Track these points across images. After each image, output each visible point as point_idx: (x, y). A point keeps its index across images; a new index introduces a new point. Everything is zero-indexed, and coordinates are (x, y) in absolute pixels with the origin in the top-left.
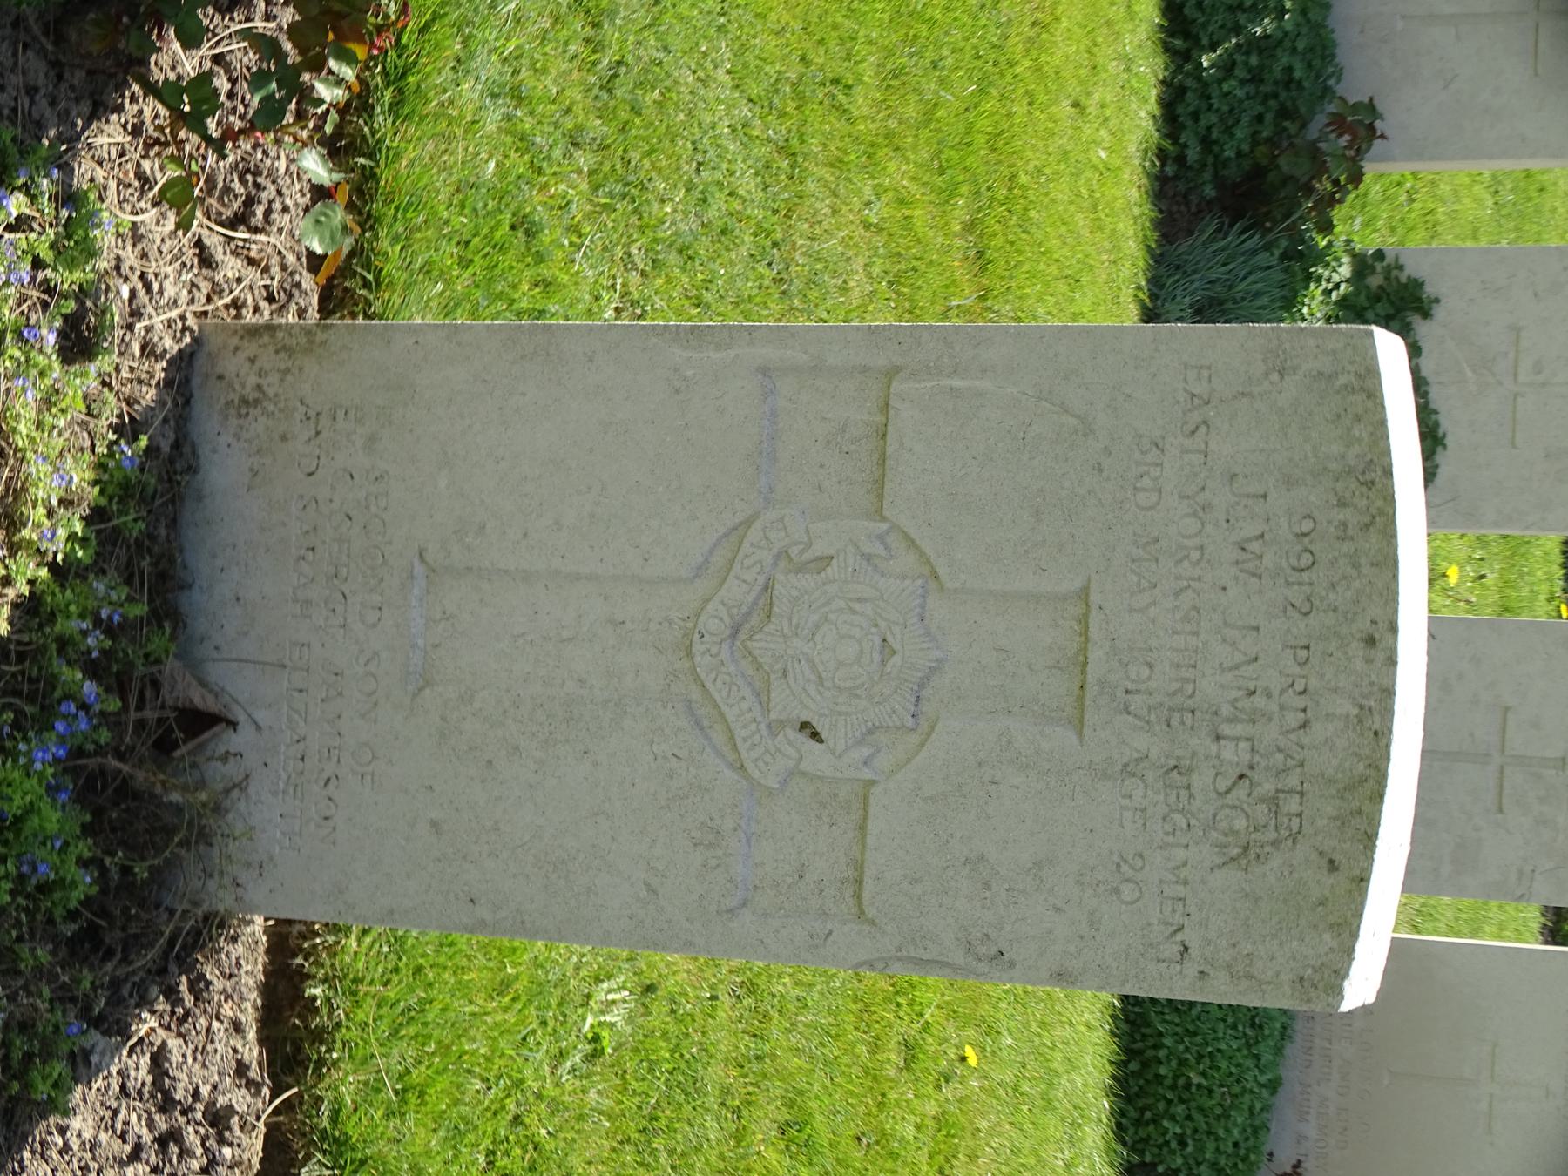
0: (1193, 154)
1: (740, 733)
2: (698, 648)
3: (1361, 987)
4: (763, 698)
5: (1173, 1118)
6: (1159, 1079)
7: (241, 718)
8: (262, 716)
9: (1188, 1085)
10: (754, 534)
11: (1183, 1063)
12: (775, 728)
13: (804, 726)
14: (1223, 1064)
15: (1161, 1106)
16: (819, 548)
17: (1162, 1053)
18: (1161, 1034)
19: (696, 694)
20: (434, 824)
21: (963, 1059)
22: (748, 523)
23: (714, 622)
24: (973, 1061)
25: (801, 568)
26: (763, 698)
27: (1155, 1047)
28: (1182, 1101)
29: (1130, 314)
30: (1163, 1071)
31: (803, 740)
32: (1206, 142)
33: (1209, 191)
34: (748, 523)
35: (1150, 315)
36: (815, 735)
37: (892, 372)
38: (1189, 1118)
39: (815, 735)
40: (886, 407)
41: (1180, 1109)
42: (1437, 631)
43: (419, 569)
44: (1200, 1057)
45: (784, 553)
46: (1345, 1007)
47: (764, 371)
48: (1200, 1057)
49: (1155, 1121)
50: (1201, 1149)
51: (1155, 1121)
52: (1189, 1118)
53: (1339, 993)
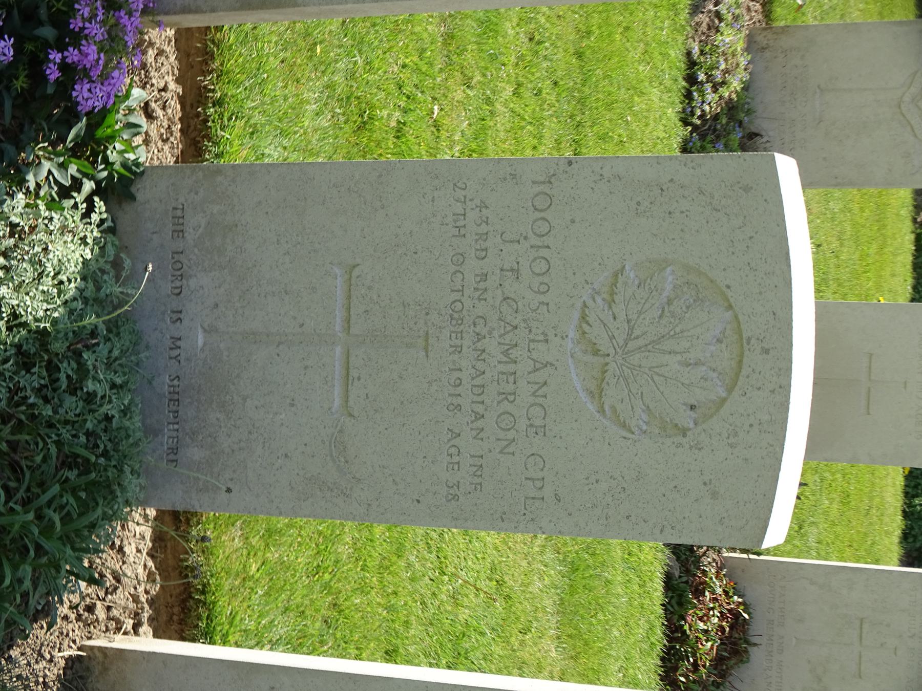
2: (902, 106)
7: (763, 133)
23: (907, 98)
43: (818, 91)
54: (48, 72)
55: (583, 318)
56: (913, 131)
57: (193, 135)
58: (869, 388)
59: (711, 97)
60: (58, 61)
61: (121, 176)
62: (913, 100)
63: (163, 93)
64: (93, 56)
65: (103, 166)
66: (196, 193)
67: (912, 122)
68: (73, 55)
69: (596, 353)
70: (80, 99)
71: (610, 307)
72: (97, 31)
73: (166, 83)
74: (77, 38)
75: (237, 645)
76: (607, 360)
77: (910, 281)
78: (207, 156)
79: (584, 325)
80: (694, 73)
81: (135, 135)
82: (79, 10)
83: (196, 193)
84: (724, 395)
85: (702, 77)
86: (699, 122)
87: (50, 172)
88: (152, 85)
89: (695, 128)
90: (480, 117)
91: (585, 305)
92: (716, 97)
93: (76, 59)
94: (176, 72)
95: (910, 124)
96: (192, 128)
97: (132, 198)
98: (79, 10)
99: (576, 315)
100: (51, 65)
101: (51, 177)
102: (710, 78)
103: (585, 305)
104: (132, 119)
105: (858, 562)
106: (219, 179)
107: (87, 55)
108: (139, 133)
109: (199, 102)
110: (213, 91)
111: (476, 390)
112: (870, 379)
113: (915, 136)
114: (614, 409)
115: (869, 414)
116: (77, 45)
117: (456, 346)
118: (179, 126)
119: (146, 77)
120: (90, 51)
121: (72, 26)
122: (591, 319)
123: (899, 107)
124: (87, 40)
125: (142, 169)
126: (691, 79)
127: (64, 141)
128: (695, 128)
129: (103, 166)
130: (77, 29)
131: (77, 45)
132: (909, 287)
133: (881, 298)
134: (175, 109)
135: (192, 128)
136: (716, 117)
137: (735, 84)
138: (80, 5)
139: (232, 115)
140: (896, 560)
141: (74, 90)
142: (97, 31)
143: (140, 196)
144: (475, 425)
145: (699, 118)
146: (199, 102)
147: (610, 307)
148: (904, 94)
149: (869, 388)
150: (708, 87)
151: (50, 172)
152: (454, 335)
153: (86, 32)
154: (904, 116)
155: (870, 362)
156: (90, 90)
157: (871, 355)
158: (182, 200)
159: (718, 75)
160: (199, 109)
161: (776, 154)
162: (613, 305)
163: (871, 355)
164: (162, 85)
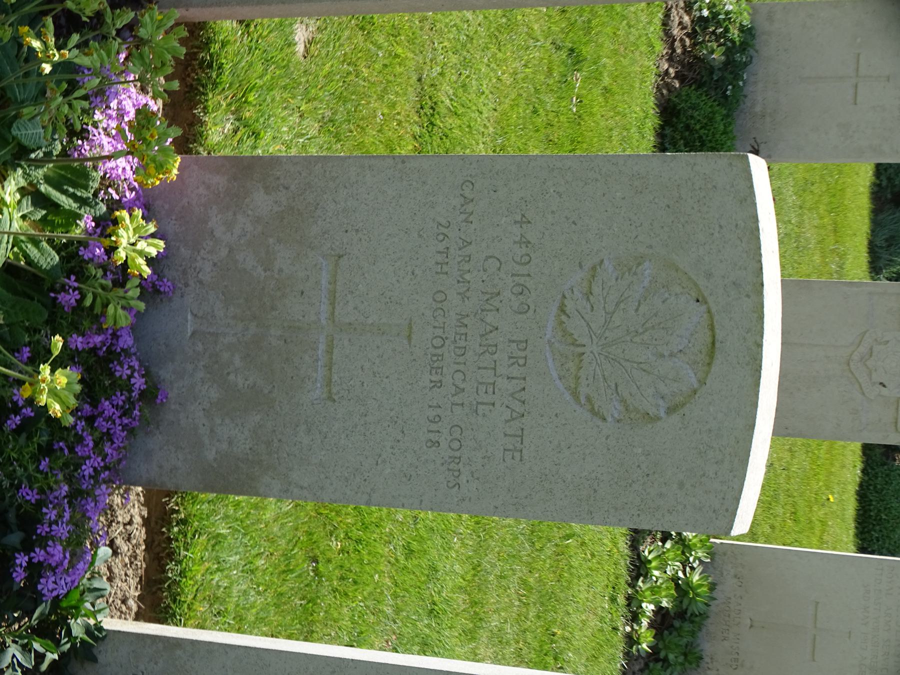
0: (884, 183)
2: (851, 364)
5: (875, 531)
6: (870, 516)
9: (881, 519)
10: (867, 335)
11: (879, 511)
13: (881, 383)
14: (893, 512)
15: (871, 526)
17: (872, 507)
18: (871, 501)
19: (850, 375)
21: (829, 499)
22: (865, 332)
23: (856, 357)
24: (832, 500)
25: (880, 344)
27: (870, 505)
28: (878, 525)
29: (643, 140)
30: (872, 514)
31: (881, 387)
32: (889, 179)
33: (889, 196)
34: (865, 332)
35: (662, 146)
36: (884, 386)
38: (881, 531)
39: (884, 386)
41: (878, 528)
44: (885, 509)
45: (876, 340)
48: (885, 509)
49: (868, 532)
50: (884, 543)
51: (868, 532)
52: (881, 531)
54: (14, 575)
55: (562, 310)
56: (861, 389)
57: (158, 550)
58: (815, 636)
60: (24, 564)
61: (83, 641)
62: (862, 359)
63: (128, 527)
64: (58, 556)
65: (66, 639)
66: (156, 663)
67: (860, 380)
68: (39, 555)
69: (574, 344)
70: (45, 591)
71: (588, 299)
72: (63, 530)
73: (132, 516)
74: (43, 542)
77: (859, 466)
78: (170, 575)
79: (563, 318)
81: (98, 597)
82: (46, 514)
83: (156, 663)
84: (696, 386)
87: (14, 656)
88: (118, 523)
89: (681, 63)
93: (42, 559)
94: (142, 499)
96: (156, 543)
97: (94, 660)
98: (46, 514)
99: (554, 310)
100: (18, 569)
101: (15, 660)
104: (96, 584)
106: (179, 652)
107: (53, 556)
108: (102, 596)
109: (163, 520)
110: (178, 512)
111: (459, 352)
112: (815, 627)
113: (863, 394)
114: (588, 399)
115: (814, 660)
116: (44, 547)
118: (144, 547)
119: (112, 516)
120: (56, 552)
121: (39, 531)
123: (848, 365)
124: (53, 541)
125: (104, 634)
127: (30, 615)
129: (66, 639)
130: (44, 534)
131: (44, 547)
133: (830, 497)
134: (140, 534)
135: (156, 543)
138: (48, 508)
139: (196, 531)
141: (40, 583)
142: (63, 530)
143: (101, 658)
146: (163, 520)
147: (588, 299)
149: (815, 636)
151: (14, 656)
153: (53, 533)
154: (852, 373)
155: (816, 610)
156: (55, 582)
157: (818, 603)
158: (142, 667)
160: (164, 530)
161: (751, 157)
162: (591, 297)
163: (818, 603)
164: (128, 519)
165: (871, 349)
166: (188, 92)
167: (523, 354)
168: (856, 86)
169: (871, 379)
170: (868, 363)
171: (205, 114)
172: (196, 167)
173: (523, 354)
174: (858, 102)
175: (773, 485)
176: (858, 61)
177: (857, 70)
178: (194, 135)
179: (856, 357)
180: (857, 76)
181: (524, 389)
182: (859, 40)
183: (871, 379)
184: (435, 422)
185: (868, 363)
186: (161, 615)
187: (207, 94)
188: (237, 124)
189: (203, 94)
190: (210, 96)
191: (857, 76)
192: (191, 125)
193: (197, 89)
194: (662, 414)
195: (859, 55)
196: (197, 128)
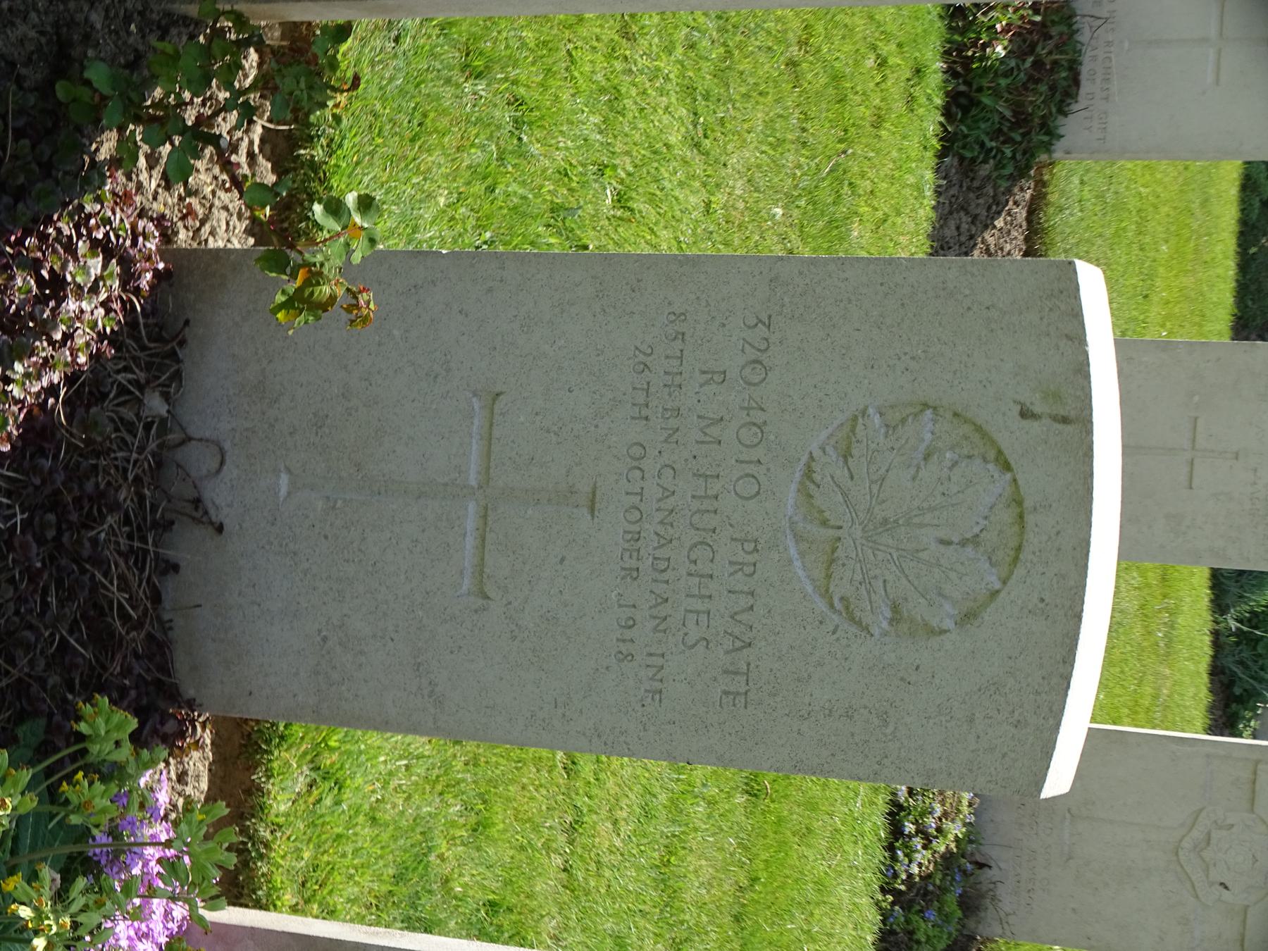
1: (1197, 885)
2: (1181, 853)
3: (1060, 778)
4: (1207, 871)
7: (992, 864)
8: (1002, 865)
10: (1203, 814)
12: (1212, 884)
13: (1222, 884)
16: (1229, 821)
19: (1179, 869)
20: (1073, 909)
22: (1201, 810)
23: (1186, 844)
25: (1220, 828)
26: (1207, 871)
31: (1221, 888)
34: (1201, 810)
36: (1226, 888)
37: (1257, 762)
39: (1226, 888)
40: (1255, 773)
42: (1125, 348)
43: (1068, 815)
46: (1043, 796)
47: (1208, 756)
53: (1040, 791)
59: (922, 856)
62: (1195, 847)
67: (1194, 878)
71: (846, 462)
75: (294, 910)
76: (839, 533)
80: (899, 821)
85: (909, 828)
86: (903, 888)
90: (700, 197)
91: (812, 458)
92: (928, 854)
95: (1190, 878)
102: (921, 831)
103: (812, 458)
105: (1154, 728)
113: (1197, 897)
117: (631, 569)
122: (817, 477)
123: (1177, 854)
126: (896, 831)
128: (897, 894)
132: (1228, 295)
136: (927, 878)
137: (955, 829)
140: (1200, 729)
144: (655, 612)
145: (903, 882)
148: (1184, 836)
150: (918, 842)
152: (627, 555)
159: (931, 822)
162: (850, 460)
165: (1209, 834)
166: (245, 746)
167: (751, 559)
168: (1192, 463)
169: (1207, 876)
170: (1204, 854)
171: (269, 778)
172: (251, 943)
173: (751, 559)
174: (1196, 482)
175: (1111, 668)
176: (1195, 428)
177: (1194, 441)
178: (252, 807)
179: (1186, 844)
180: (1193, 448)
181: (751, 608)
182: (1196, 398)
183: (1207, 876)
184: (630, 627)
185: (1204, 854)
186: (238, 888)
187: (271, 753)
188: (314, 775)
189: (266, 752)
190: (276, 753)
191: (1193, 448)
192: (248, 792)
193: (256, 743)
194: (948, 624)
195: (1196, 419)
196: (255, 800)
